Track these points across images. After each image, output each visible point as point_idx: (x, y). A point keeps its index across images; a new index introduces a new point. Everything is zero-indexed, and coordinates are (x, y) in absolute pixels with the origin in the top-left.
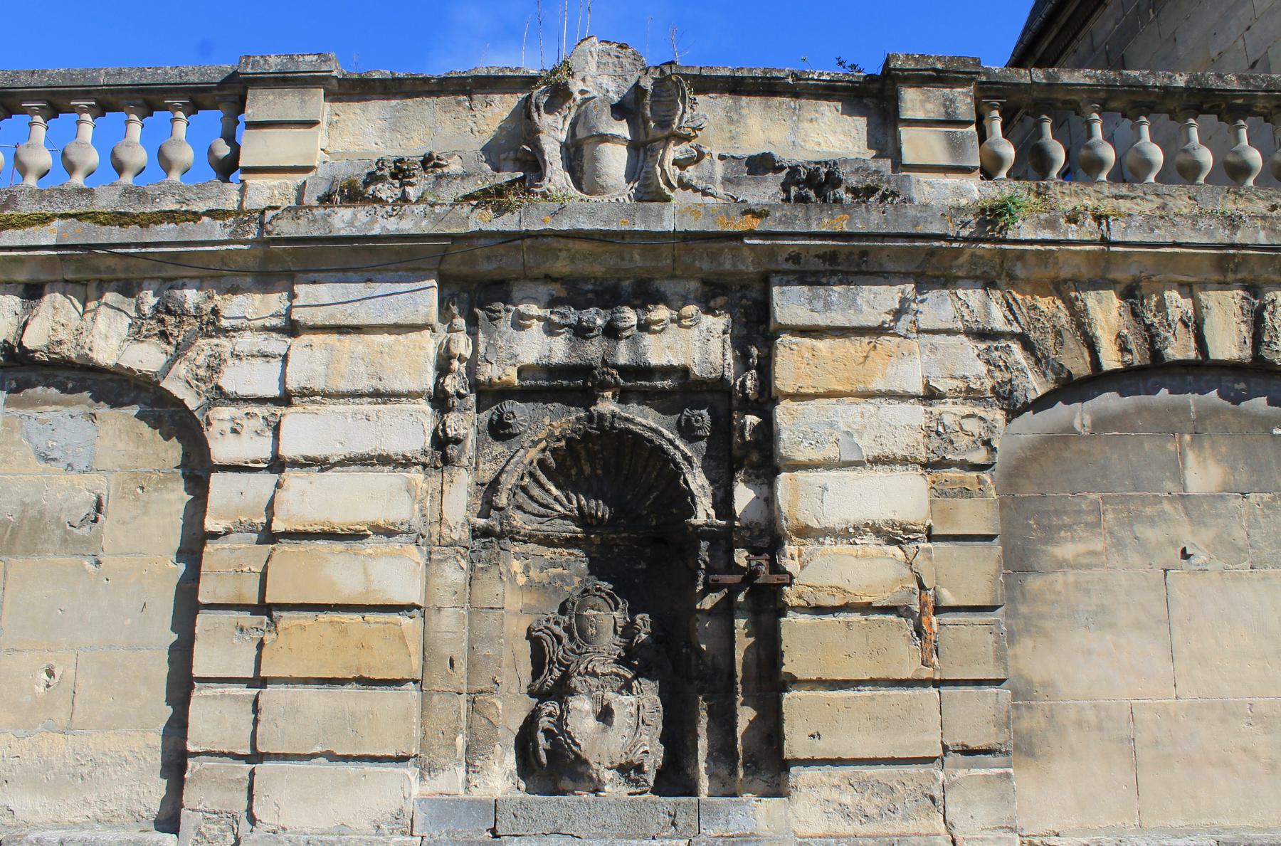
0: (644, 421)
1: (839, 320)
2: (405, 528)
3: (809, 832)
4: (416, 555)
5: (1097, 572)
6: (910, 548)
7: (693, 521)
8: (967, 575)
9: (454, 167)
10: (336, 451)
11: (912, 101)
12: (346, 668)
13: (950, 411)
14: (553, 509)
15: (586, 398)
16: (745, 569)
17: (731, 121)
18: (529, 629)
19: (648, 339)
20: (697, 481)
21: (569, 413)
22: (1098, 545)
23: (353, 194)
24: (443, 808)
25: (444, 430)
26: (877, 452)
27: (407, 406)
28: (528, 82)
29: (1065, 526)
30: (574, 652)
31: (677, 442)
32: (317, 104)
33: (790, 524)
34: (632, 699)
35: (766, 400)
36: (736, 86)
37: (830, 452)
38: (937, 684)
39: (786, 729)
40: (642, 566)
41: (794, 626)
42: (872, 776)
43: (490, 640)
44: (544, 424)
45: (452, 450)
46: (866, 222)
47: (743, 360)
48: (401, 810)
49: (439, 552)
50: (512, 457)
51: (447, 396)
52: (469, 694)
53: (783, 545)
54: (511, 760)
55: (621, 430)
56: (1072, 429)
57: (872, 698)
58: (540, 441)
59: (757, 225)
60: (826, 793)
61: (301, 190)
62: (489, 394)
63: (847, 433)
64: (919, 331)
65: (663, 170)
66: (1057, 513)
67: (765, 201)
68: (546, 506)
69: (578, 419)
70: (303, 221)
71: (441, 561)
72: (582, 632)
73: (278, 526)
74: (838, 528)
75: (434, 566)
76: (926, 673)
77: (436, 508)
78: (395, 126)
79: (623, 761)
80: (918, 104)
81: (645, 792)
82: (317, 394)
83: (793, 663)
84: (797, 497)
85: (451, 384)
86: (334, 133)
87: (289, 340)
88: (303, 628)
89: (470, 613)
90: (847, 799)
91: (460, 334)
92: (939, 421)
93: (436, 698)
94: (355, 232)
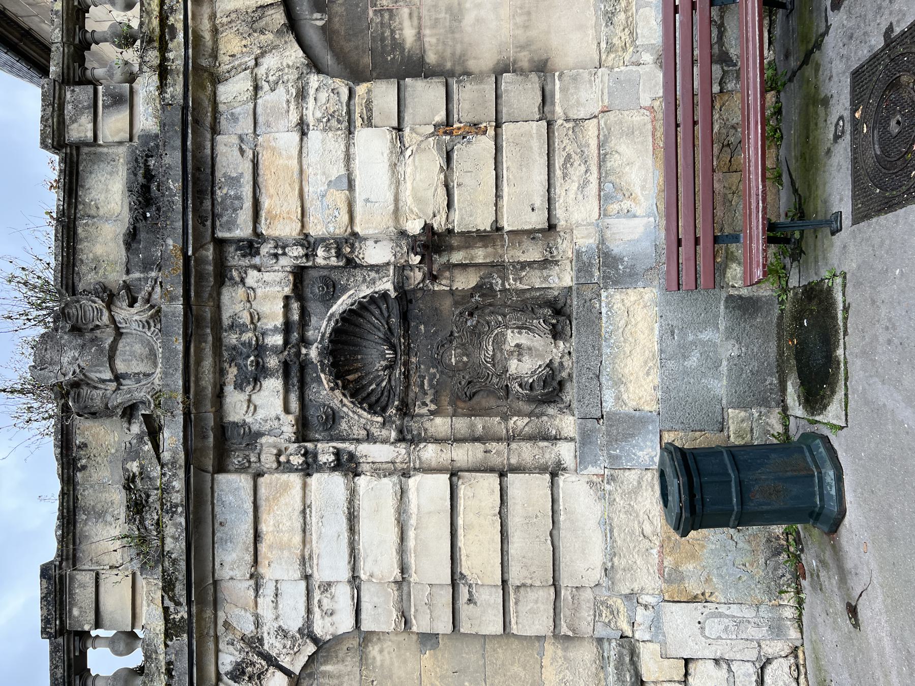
1: (247, 191)
5: (424, 12)
8: (427, 97)
13: (312, 112)
22: (405, 11)
27: (314, 497)
29: (392, 34)
38: (498, 126)
40: (422, 327)
41: (461, 221)
55: (331, 341)
56: (323, 28)
62: (303, 432)
66: (383, 39)
76: (491, 132)
78: (100, 515)
83: (484, 223)
92: (319, 121)
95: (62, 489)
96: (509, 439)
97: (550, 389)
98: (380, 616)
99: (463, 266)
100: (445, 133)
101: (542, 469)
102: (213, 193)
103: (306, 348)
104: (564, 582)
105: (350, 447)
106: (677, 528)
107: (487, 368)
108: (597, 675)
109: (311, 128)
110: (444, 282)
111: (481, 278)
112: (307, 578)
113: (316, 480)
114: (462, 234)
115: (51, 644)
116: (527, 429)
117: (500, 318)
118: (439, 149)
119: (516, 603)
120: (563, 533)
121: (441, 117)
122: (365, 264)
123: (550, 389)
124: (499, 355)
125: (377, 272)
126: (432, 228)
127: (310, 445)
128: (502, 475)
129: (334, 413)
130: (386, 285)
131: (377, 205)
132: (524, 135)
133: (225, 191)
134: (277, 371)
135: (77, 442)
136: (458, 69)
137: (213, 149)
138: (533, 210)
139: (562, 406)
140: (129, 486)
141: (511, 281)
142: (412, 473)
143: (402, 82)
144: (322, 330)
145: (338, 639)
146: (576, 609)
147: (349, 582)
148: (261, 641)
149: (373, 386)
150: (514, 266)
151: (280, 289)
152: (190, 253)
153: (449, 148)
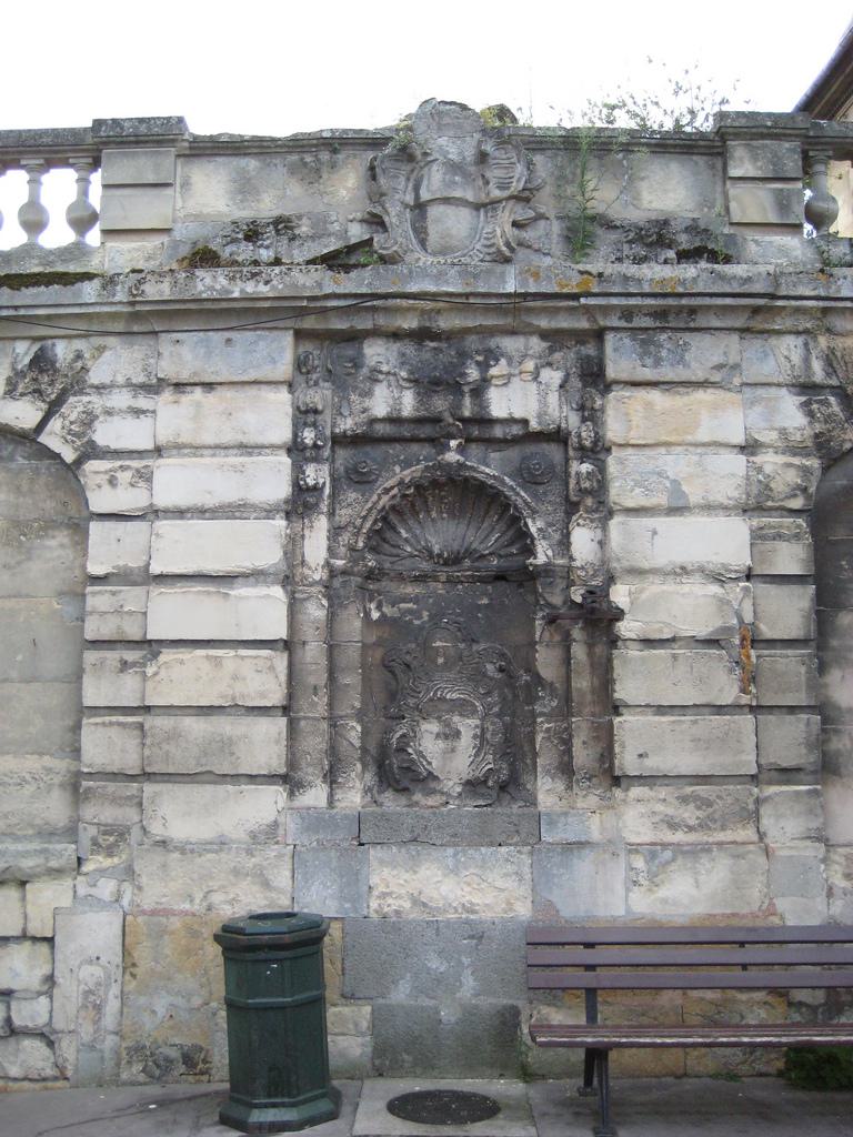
8: (788, 612)
40: (485, 601)
76: (745, 699)
83: (625, 690)
95: (280, 139)
96: (333, 721)
97: (397, 772)
98: (107, 549)
99: (567, 660)
100: (743, 639)
101: (292, 763)
102: (663, 329)
104: (149, 789)
105: (324, 507)
106: (226, 929)
107: (428, 691)
108: (32, 826)
109: (752, 459)
110: (547, 634)
111: (552, 684)
112: (158, 451)
113: (285, 461)
114: (610, 660)
115: (85, 129)
117: (496, 709)
118: (716, 631)
119: (104, 724)
121: (767, 632)
122: (571, 527)
123: (397, 772)
124: (445, 707)
125: (560, 543)
126: (618, 620)
127: (326, 453)
128: (286, 710)
129: (369, 482)
130: (543, 554)
132: (741, 745)
134: (426, 410)
136: (828, 656)
138: (641, 756)
139: (375, 792)
140: (281, 222)
141: (546, 725)
142: (289, 588)
143: (810, 579)
144: (483, 468)
145: (80, 494)
146: (116, 800)
147: (151, 505)
148: (81, 392)
149: (404, 534)
150: (566, 729)
152: (583, 300)
153: (723, 643)
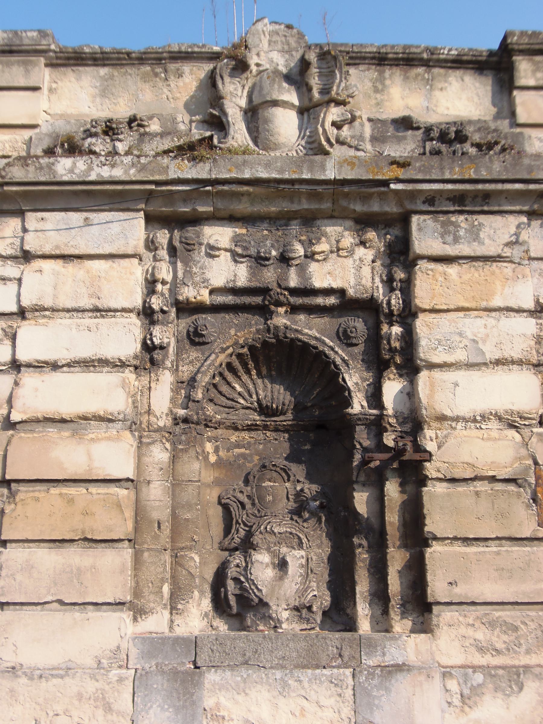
0: (310, 332)
1: (464, 249)
2: (121, 417)
3: (450, 663)
4: (129, 441)
6: (526, 432)
7: (350, 410)
9: (154, 127)
10: (62, 355)
11: (525, 70)
12: (73, 531)
14: (237, 402)
15: (264, 311)
16: (391, 448)
17: (376, 90)
18: (219, 497)
19: (313, 267)
20: (355, 379)
21: (250, 326)
23: (73, 149)
24: (153, 645)
25: (151, 339)
26: (497, 355)
27: (121, 320)
28: (215, 57)
30: (256, 516)
31: (336, 349)
32: (43, 75)
33: (429, 413)
34: (303, 553)
35: (408, 314)
36: (381, 60)
37: (460, 356)
39: (429, 578)
40: (308, 447)
42: (500, 617)
43: (189, 506)
44: (234, 334)
45: (157, 355)
46: (489, 170)
47: (389, 281)
48: (118, 647)
49: (148, 437)
50: (205, 360)
51: (153, 311)
52: (172, 550)
53: (422, 429)
54: (207, 604)
55: (292, 340)
57: (498, 553)
58: (228, 348)
59: (401, 173)
60: (463, 630)
61: (29, 142)
62: (185, 308)
63: (474, 340)
64: (530, 259)
65: (324, 130)
67: (406, 155)
68: (232, 400)
69: (258, 331)
70: (31, 169)
71: (149, 444)
72: (261, 499)
73: (15, 417)
74: (467, 416)
75: (144, 448)
77: (145, 401)
78: (105, 92)
79: (297, 604)
80: (530, 73)
81: (313, 628)
82: (46, 309)
83: (433, 524)
84: (436, 392)
85: (156, 303)
86: (53, 97)
87: (22, 267)
88: (37, 499)
89: (173, 485)
90: (480, 636)
91: (162, 262)
93: (146, 554)
94: (75, 178)
97: (236, 604)
101: (137, 593)
102: (461, 212)
103: (286, 312)
113: (135, 324)
116: (184, 572)
120: (59, 616)
131: (452, 395)
133: (463, 225)
134: (257, 280)
135: (184, 68)
137: (511, 212)
149: (238, 388)
151: (352, 284)
152: (392, 186)
